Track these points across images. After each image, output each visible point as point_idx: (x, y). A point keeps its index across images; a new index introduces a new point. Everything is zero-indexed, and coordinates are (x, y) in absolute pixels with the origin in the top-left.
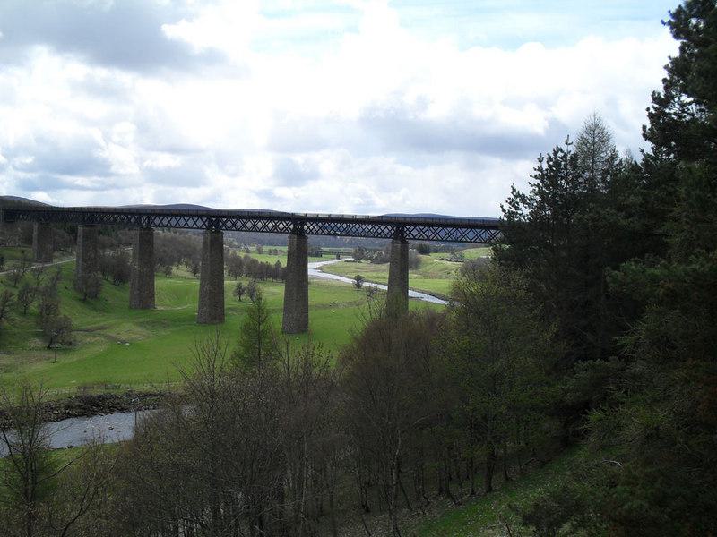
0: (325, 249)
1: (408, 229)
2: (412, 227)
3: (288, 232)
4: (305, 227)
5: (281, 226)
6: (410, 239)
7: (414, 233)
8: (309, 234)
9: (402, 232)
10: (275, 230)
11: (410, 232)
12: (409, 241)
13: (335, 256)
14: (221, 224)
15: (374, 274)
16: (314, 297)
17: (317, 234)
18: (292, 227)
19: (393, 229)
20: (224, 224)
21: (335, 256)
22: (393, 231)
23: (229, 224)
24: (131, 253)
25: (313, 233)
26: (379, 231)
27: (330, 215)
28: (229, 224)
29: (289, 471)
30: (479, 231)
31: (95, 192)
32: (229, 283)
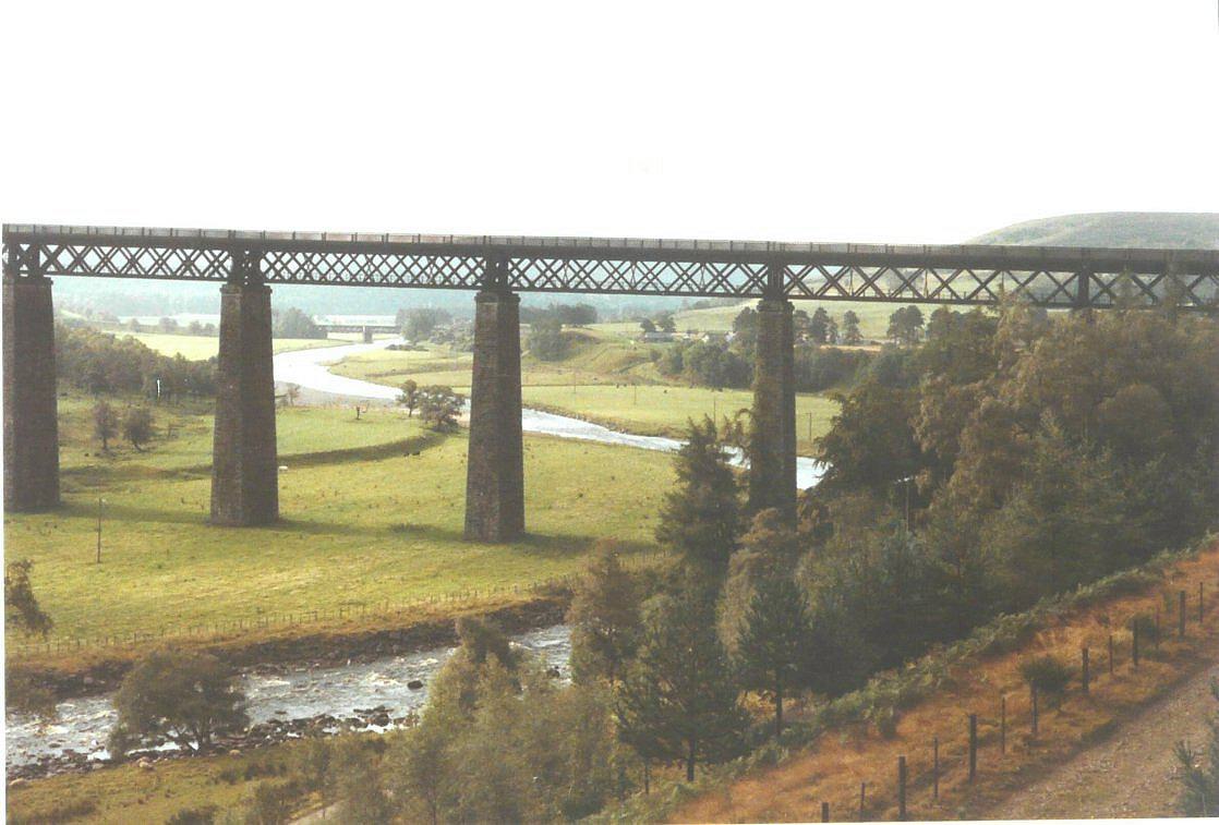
0: (331, 320)
1: (515, 266)
2: (527, 262)
3: (221, 278)
4: (264, 266)
5: (202, 263)
6: (522, 288)
7: (532, 273)
8: (273, 281)
9: (505, 272)
10: (187, 272)
11: (522, 273)
12: (521, 294)
13: (360, 336)
14: (43, 258)
15: (444, 361)
16: (533, 463)
17: (293, 280)
18: (229, 264)
19: (479, 265)
20: (52, 258)
21: (360, 336)
22: (479, 272)
23: (65, 259)
24: (562, 662)
25: (283, 281)
26: (447, 271)
27: (355, 236)
28: (65, 259)
29: (659, 739)
30: (685, 265)
31: (1053, 283)
32: (72, 406)
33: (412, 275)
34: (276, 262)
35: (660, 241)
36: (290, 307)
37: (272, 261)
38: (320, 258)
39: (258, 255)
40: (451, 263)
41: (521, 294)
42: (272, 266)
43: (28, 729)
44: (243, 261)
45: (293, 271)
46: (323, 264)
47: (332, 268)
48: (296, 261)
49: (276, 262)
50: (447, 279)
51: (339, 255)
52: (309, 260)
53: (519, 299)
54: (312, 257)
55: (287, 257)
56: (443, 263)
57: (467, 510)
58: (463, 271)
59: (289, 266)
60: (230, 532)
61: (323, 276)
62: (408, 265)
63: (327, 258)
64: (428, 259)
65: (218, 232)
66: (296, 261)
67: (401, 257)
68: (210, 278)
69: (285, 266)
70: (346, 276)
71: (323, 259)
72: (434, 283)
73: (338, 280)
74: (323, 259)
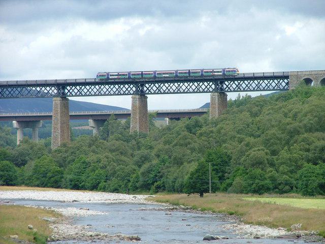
8: (228, 91)
39: (64, 88)
58: (203, 87)
65: (72, 80)
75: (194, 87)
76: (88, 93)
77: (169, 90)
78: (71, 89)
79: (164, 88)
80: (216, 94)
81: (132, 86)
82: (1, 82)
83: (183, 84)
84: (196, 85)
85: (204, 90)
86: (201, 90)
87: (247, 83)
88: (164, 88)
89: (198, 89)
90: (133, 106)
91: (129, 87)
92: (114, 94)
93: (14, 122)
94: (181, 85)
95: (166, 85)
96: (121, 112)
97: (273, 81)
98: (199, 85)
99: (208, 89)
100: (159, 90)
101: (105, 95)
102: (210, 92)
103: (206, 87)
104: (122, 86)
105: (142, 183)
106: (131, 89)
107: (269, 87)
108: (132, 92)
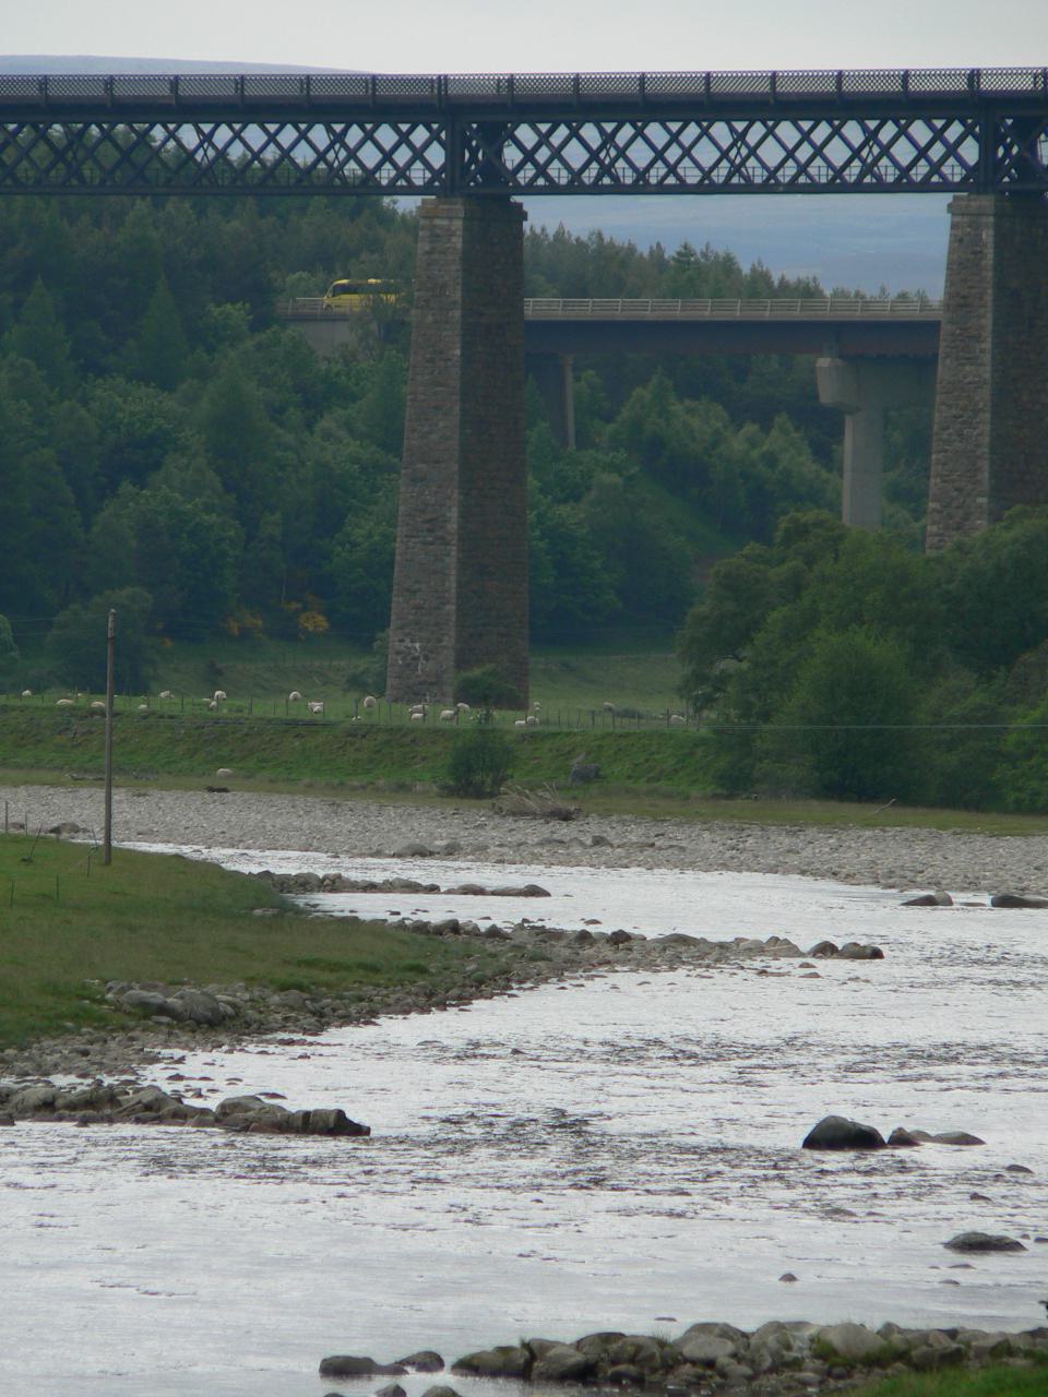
4: (511, 155)
8: (530, 189)
25: (553, 189)
33: (829, 165)
34: (396, 147)
35: (774, 76)
36: (722, 254)
37: (660, 145)
38: (295, 134)
39: (498, 134)
40: (412, 137)
41: (529, 203)
42: (529, 156)
43: (446, 1368)
44: (1001, 141)
45: (838, 163)
46: (774, 146)
47: (387, 156)
48: (310, 143)
49: (396, 147)
50: (402, 172)
51: (272, 128)
52: (871, 136)
53: (524, 216)
54: (345, 132)
55: (823, 130)
56: (395, 138)
57: (128, 694)
58: (903, 152)
59: (428, 154)
60: (445, 800)
61: (642, 174)
62: (387, 147)
63: (311, 135)
64: (329, 130)
66: (310, 143)
67: (237, 127)
68: (924, 187)
69: (557, 153)
70: (693, 176)
71: (303, 136)
72: (647, 182)
73: (541, 182)
74: (303, 136)
75: (837, 153)
76: (660, 170)
77: (672, 169)
78: (544, 139)
79: (640, 154)
80: (987, 202)
81: (420, 135)
82: (4, 58)
83: (705, 132)
84: (725, 139)
85: (905, 171)
86: (890, 175)
87: (660, 142)
88: (640, 154)
89: (606, 170)
90: (961, 265)
91: (938, 135)
92: (837, 184)
93: (824, 362)
94: (752, 138)
95: (656, 132)
96: (767, 312)
97: (640, 133)
98: (740, 137)
99: (936, 168)
100: (606, 170)
101: (770, 186)
102: (945, 186)
103: (790, 154)
104: (354, 135)
105: (199, 1052)
106: (952, 150)
107: (803, 169)
108: (418, 175)
